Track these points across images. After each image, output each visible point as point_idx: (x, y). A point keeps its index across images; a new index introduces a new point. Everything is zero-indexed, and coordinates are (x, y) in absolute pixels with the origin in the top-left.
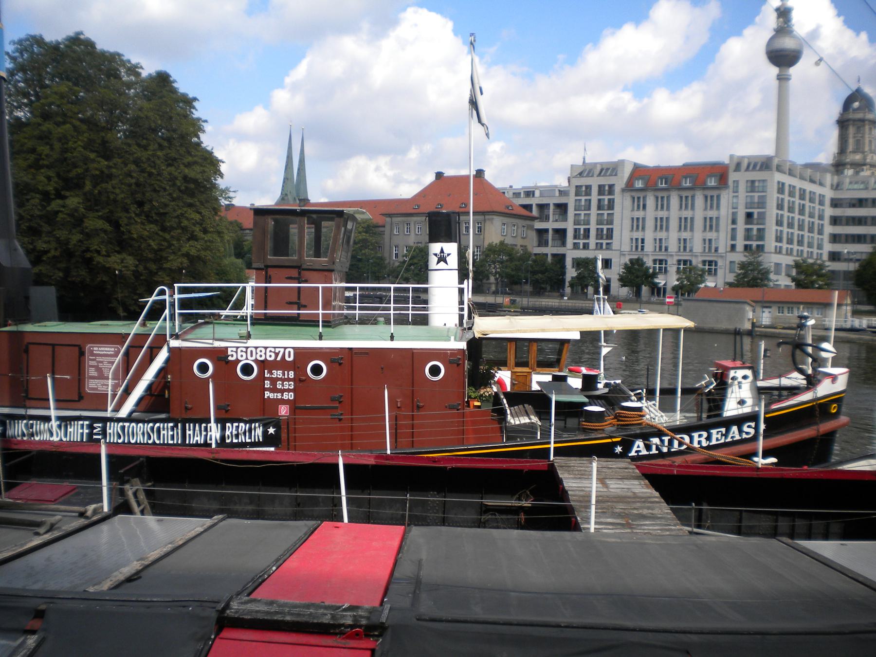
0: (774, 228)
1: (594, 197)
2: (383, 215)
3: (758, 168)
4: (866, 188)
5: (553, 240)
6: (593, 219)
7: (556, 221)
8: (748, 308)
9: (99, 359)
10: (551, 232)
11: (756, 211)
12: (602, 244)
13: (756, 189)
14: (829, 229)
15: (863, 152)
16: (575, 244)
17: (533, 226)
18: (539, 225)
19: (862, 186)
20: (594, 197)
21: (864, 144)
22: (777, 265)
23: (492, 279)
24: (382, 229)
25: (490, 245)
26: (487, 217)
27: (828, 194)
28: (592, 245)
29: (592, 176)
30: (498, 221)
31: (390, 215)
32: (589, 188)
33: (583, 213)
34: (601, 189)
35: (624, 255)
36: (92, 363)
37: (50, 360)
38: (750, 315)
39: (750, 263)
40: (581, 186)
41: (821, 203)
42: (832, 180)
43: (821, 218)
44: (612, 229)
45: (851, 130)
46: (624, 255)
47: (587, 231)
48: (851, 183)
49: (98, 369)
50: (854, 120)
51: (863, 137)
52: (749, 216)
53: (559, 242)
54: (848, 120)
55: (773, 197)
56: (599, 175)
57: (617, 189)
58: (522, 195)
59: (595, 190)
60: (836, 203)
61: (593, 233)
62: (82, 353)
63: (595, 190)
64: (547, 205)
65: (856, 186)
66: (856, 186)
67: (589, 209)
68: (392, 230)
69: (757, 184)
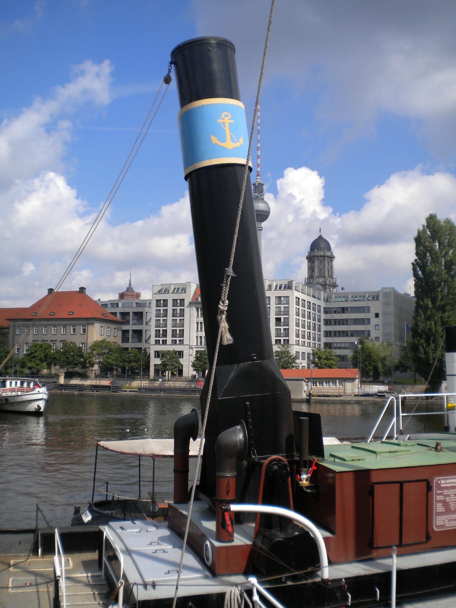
0: (295, 328)
1: (170, 308)
2: (7, 320)
3: (283, 288)
4: (347, 301)
5: (132, 338)
6: (170, 323)
7: (135, 324)
8: (304, 383)
9: (446, 492)
10: (131, 332)
11: (282, 317)
12: (176, 340)
13: (282, 303)
14: (323, 328)
15: (324, 277)
16: (156, 341)
17: (121, 328)
18: (125, 327)
19: (343, 299)
20: (170, 308)
21: (324, 272)
22: (297, 352)
23: (96, 367)
24: (7, 330)
25: (95, 342)
26: (90, 322)
27: (323, 304)
28: (169, 341)
29: (168, 293)
30: (97, 326)
31: (13, 320)
32: (166, 301)
33: (161, 319)
34: (175, 301)
35: (192, 348)
36: (439, 498)
37: (397, 499)
38: (305, 388)
39: (282, 353)
40: (160, 300)
41: (319, 311)
42: (324, 295)
43: (319, 321)
44: (183, 330)
45: (317, 263)
46: (192, 348)
47: (165, 332)
48: (336, 297)
49: (445, 504)
50: (318, 257)
51: (324, 267)
52: (278, 320)
53: (136, 340)
54: (314, 256)
55: (293, 307)
56: (173, 293)
57: (186, 303)
58: (109, 306)
59: (170, 303)
60: (327, 311)
61: (169, 333)
62: (429, 488)
63: (170, 303)
64: (128, 314)
65: (339, 300)
66: (339, 300)
67: (166, 316)
68: (14, 332)
69: (282, 299)
